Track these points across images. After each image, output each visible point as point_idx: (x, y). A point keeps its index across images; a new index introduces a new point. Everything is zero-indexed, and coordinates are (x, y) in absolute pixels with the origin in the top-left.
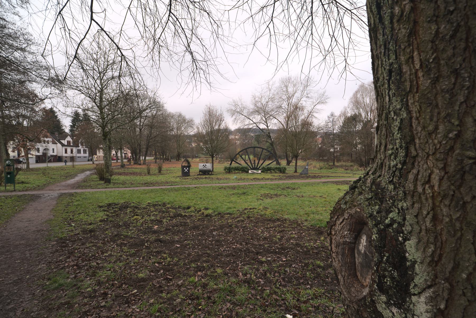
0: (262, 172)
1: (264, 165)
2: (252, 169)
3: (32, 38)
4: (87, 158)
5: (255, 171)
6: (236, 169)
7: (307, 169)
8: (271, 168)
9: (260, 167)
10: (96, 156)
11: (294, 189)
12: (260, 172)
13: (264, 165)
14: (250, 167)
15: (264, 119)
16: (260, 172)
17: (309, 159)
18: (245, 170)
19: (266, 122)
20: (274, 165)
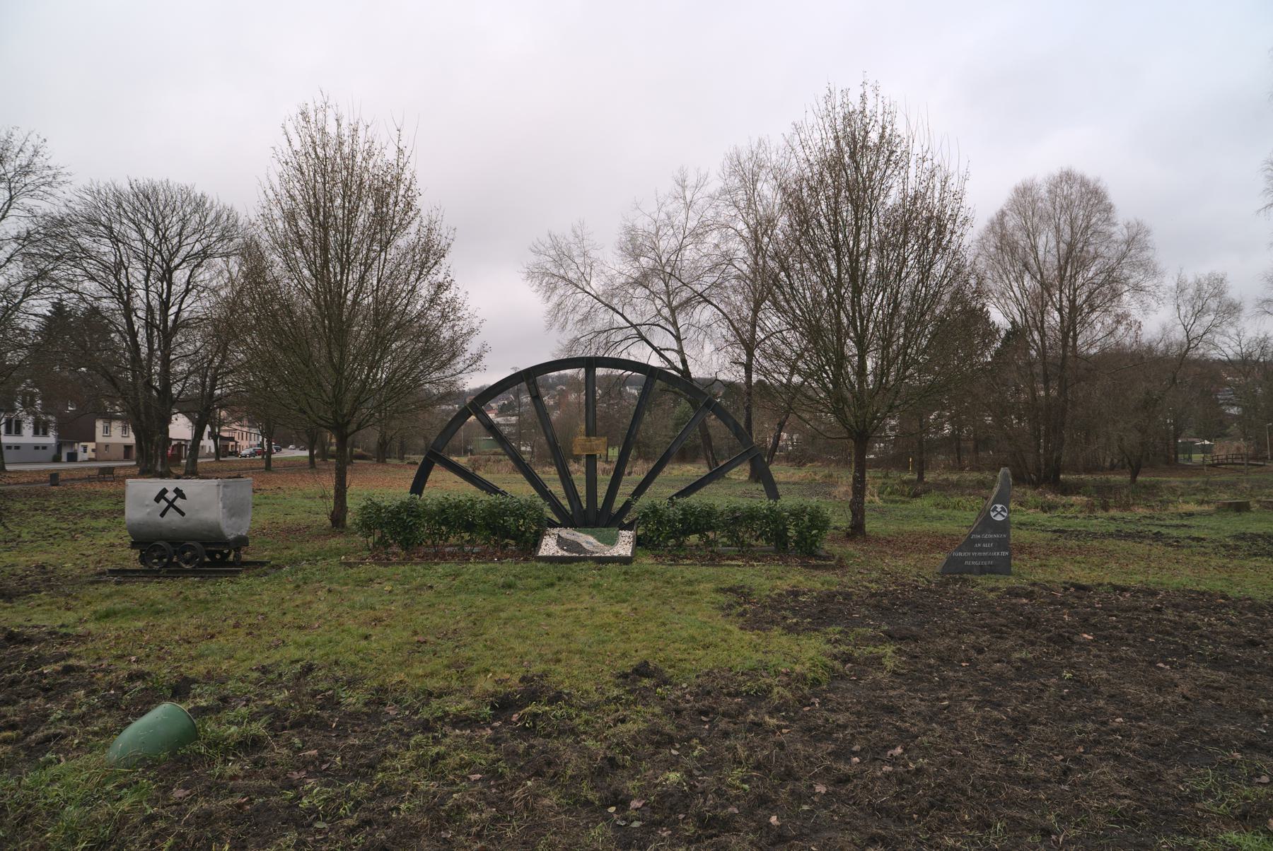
0: (639, 542)
1: (659, 494)
2: (568, 521)
3: (277, 213)
4: (52, 452)
5: (587, 541)
6: (454, 518)
7: (1004, 527)
8: (710, 513)
9: (627, 506)
10: (91, 446)
11: (313, 142)
12: (624, 546)
13: (659, 494)
14: (556, 507)
15: (666, 312)
16: (624, 546)
17: (812, 461)
18: (508, 533)
19: (675, 324)
20: (734, 492)
